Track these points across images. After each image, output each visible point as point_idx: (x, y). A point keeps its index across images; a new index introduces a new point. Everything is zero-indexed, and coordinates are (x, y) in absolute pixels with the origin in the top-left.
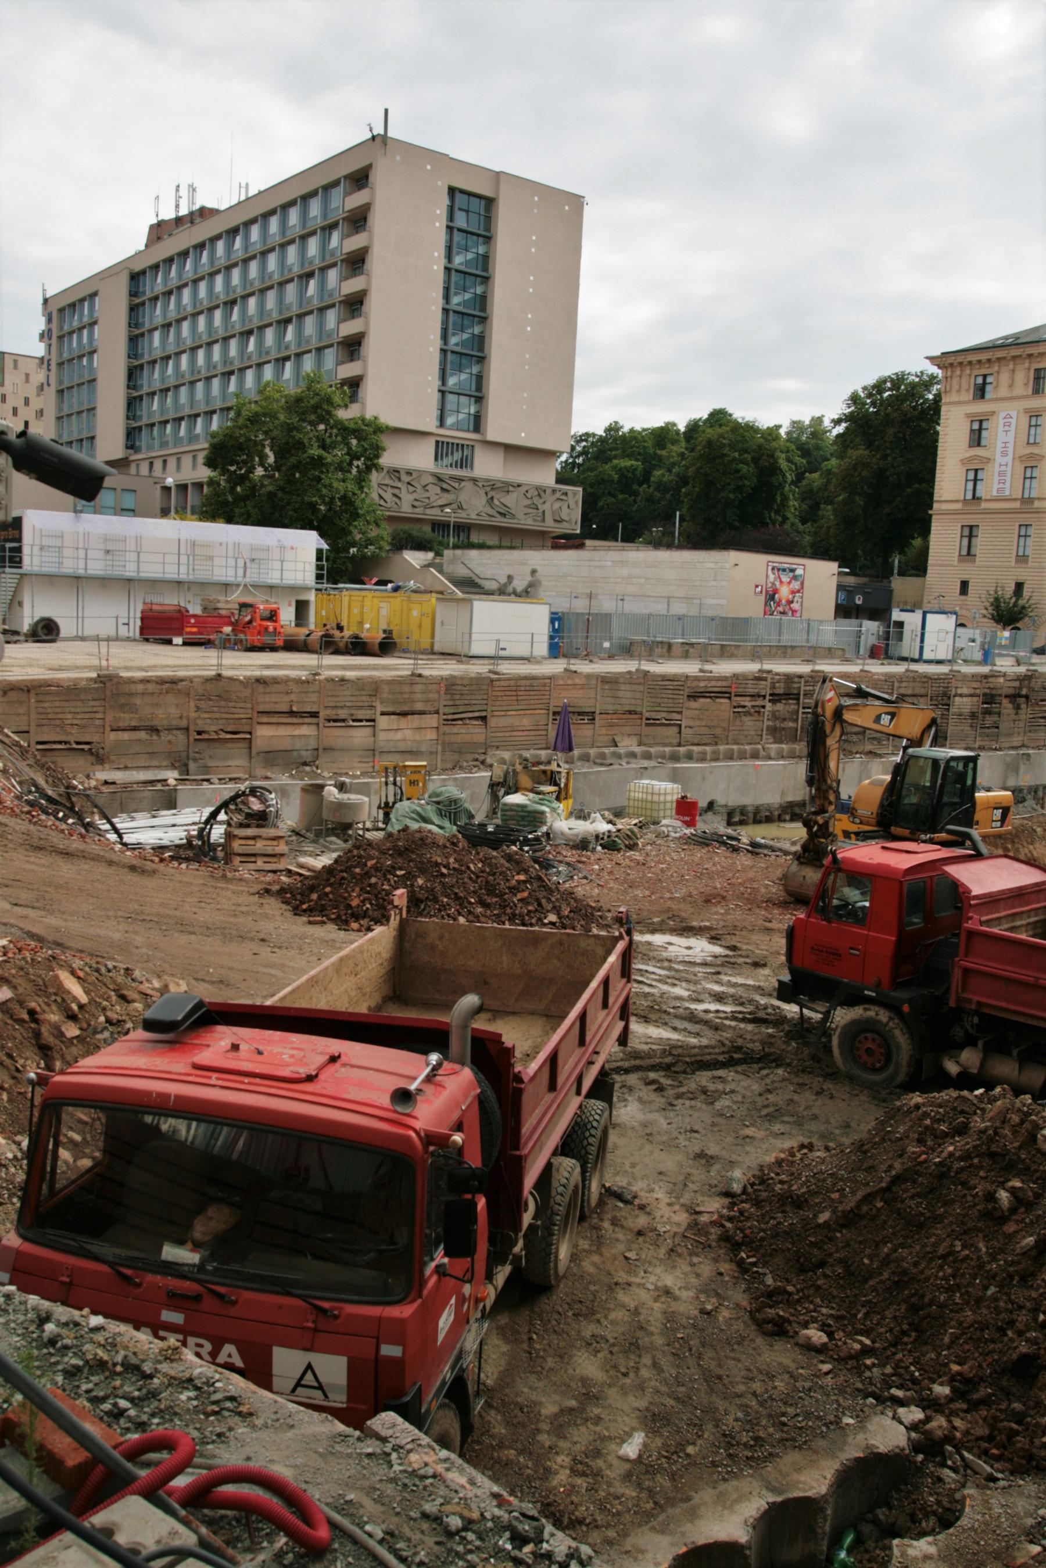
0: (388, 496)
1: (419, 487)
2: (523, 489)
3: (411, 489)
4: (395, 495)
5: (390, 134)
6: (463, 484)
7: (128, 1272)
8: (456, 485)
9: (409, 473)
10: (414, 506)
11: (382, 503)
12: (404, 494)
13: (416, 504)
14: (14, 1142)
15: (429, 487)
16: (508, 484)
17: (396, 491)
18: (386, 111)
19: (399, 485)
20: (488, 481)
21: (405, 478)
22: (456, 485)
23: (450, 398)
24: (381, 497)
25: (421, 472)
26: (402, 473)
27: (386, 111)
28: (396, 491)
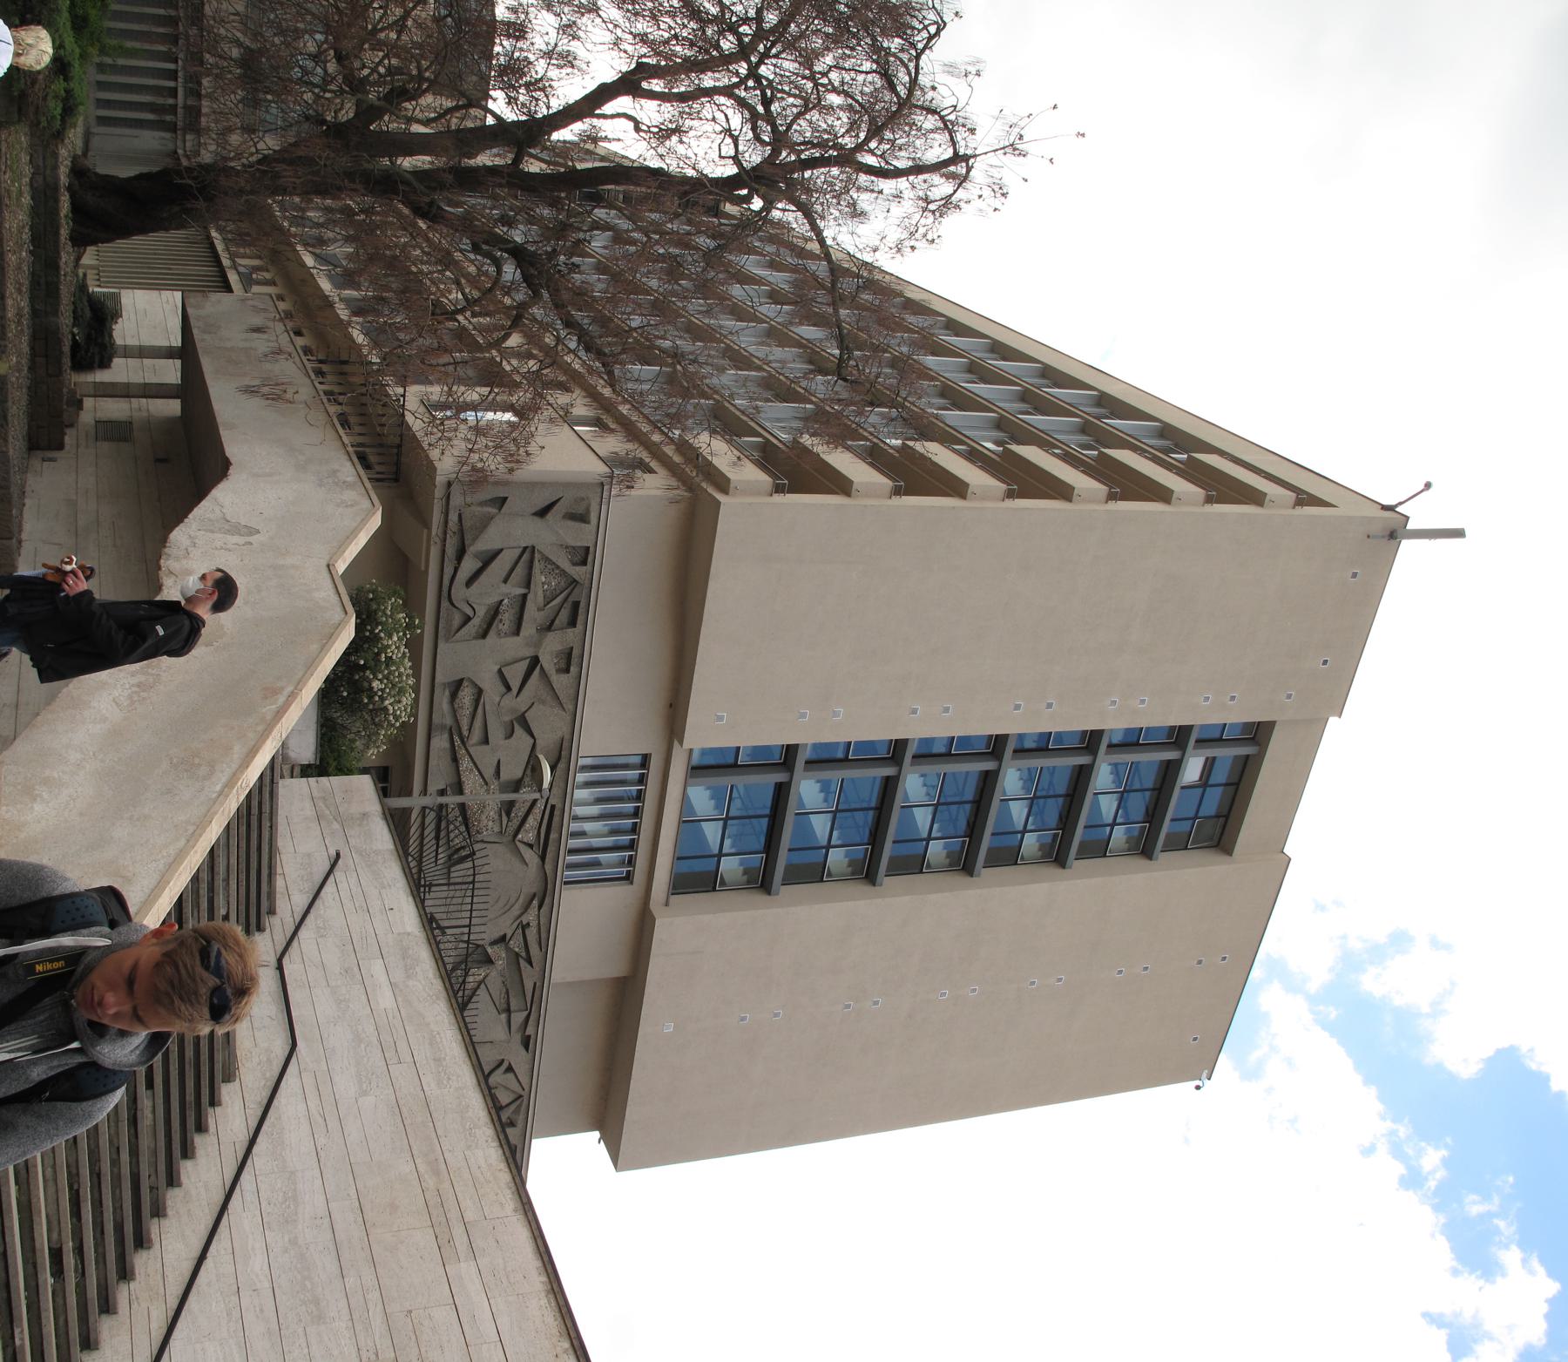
0: (493, 589)
1: (521, 703)
2: (518, 1058)
3: (515, 675)
4: (495, 613)
5: (1224, 782)
6: (531, 856)
7: (463, 281)
8: (528, 835)
9: (570, 660)
10: (458, 684)
11: (469, 565)
12: (508, 648)
13: (466, 696)
14: (639, 35)
15: (521, 739)
16: (533, 1003)
17: (507, 617)
18: (1458, 533)
19: (528, 629)
20: (543, 944)
21: (549, 651)
22: (528, 835)
23: (452, 881)
24: (489, 559)
25: (571, 706)
26: (571, 635)
27: (1458, 533)
28: (507, 617)
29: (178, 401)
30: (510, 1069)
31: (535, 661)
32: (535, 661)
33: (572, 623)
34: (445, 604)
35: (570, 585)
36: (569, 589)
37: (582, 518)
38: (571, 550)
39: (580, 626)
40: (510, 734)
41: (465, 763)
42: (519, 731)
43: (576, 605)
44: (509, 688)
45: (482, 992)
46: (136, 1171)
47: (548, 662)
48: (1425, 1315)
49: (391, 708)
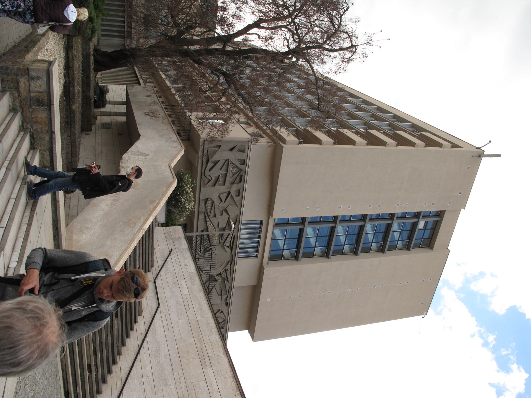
3: (223, 197)
11: (210, 165)
24: (216, 163)
32: (229, 193)
33: (240, 182)
34: (203, 176)
37: (243, 151)
40: (222, 214)
41: (209, 223)
43: (241, 176)
44: (222, 201)
47: (233, 193)
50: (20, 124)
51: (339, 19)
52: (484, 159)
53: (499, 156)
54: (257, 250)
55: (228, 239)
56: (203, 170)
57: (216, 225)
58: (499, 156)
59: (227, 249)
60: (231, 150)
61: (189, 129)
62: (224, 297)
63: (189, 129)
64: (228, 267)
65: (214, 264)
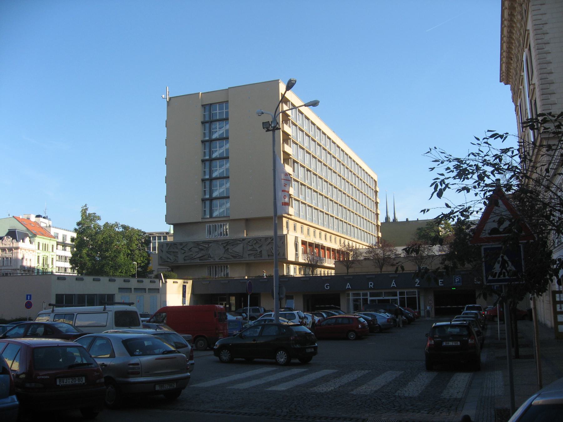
3: (183, 251)
11: (169, 260)
19: (177, 251)
24: (168, 258)
29: (231, 297)
30: (249, 242)
31: (181, 249)
32: (181, 249)
33: (176, 244)
34: (173, 263)
35: (200, 245)
36: (201, 244)
37: (163, 245)
38: (167, 246)
39: (176, 243)
40: (191, 251)
41: (195, 257)
42: (191, 250)
43: (174, 244)
44: (185, 252)
45: (233, 249)
46: (474, 314)
47: (181, 247)
48: (551, 63)
49: (540, 255)
50: (27, 368)
51: (485, 191)
52: (286, 95)
53: (471, 143)
54: (8, 249)
55: (204, 246)
56: (170, 263)
57: (197, 253)
58: (471, 143)
59: (210, 245)
60: (162, 251)
61: (279, 247)
62: (239, 242)
63: (279, 247)
64: (220, 243)
65: (349, 230)
